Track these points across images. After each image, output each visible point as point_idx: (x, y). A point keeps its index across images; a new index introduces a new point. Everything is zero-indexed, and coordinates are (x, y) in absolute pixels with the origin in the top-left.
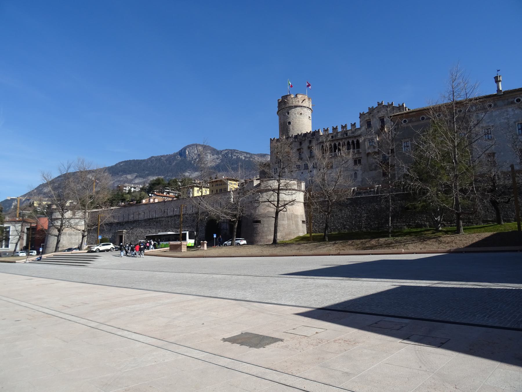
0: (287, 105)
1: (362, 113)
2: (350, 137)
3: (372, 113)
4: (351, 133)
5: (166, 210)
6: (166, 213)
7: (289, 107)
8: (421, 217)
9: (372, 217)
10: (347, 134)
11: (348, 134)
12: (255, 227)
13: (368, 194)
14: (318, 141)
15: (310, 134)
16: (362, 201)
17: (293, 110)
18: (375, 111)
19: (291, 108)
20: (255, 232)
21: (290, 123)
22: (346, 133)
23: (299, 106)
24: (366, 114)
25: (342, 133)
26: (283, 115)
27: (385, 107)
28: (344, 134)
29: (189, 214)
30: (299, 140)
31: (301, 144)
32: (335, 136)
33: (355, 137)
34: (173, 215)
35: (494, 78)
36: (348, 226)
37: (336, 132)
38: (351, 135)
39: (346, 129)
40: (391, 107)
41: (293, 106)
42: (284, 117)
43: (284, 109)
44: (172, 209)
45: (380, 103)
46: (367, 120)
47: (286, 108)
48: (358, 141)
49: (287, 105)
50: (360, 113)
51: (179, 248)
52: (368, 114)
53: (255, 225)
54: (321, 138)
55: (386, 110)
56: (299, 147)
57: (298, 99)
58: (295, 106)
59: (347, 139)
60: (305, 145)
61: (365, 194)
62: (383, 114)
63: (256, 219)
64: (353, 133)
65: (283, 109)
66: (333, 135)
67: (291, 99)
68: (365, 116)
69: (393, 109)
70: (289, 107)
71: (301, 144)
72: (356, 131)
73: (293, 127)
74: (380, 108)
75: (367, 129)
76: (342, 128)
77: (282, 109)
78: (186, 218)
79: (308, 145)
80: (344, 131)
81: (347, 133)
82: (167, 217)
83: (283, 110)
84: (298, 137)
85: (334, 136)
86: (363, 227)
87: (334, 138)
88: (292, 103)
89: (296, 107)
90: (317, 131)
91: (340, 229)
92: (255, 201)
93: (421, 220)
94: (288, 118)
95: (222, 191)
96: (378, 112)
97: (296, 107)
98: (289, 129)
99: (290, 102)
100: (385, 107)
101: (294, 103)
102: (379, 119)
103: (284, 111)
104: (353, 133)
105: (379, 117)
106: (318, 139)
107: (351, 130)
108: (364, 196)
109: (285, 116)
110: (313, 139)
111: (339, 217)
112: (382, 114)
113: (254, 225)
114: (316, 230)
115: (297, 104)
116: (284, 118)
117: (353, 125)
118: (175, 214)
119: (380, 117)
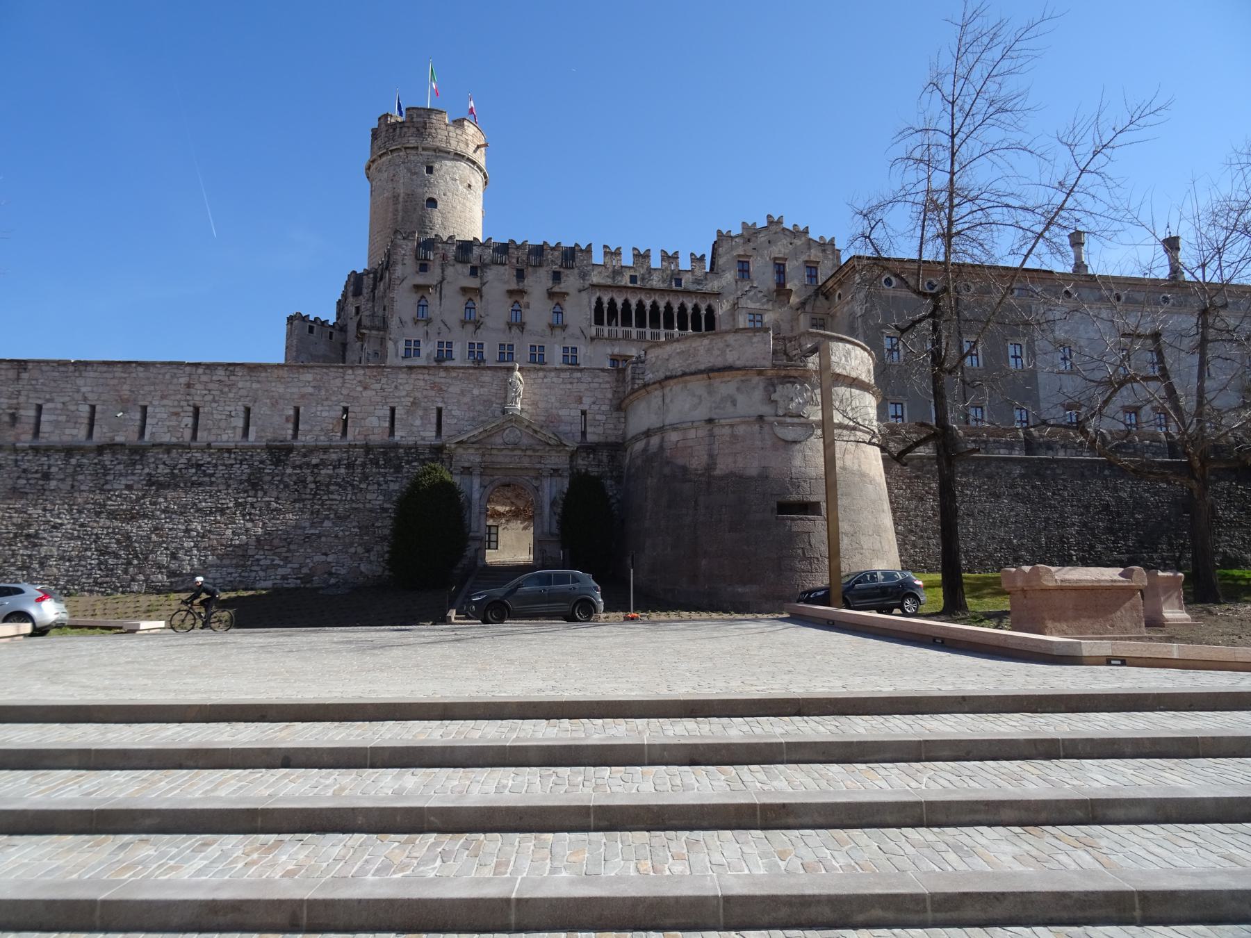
0: (429, 142)
1: (724, 233)
2: (688, 293)
3: (753, 239)
4: (693, 283)
5: (32, 413)
6: (26, 428)
7: (435, 150)
8: (1229, 536)
9: (1098, 527)
10: (679, 282)
11: (683, 282)
12: (795, 529)
13: (1074, 451)
14: (584, 280)
15: (556, 253)
16: (1058, 471)
17: (449, 163)
18: (762, 238)
19: (442, 154)
20: (800, 551)
21: (432, 203)
22: (677, 277)
23: (468, 159)
24: (737, 240)
25: (665, 276)
26: (409, 170)
27: (787, 232)
28: (671, 278)
29: (220, 450)
30: (514, 261)
31: (520, 275)
32: (643, 279)
33: (705, 295)
34: (88, 444)
35: (291, 319)
36: (1026, 550)
37: (645, 267)
38: (693, 287)
39: (677, 265)
40: (803, 239)
41: (449, 153)
42: (415, 177)
43: (414, 152)
44: (85, 409)
45: (776, 219)
46: (739, 256)
47: (424, 149)
48: (710, 310)
49: (429, 142)
50: (719, 232)
51: (1118, 607)
52: (742, 241)
53: (793, 520)
54: (595, 273)
55: (791, 244)
56: (514, 286)
57: (467, 134)
58: (456, 154)
59: (666, 294)
60: (538, 283)
61: (1065, 452)
62: (783, 250)
63: (794, 497)
64: (697, 282)
65: (408, 148)
66: (637, 274)
67: (444, 127)
68: (734, 243)
69: (809, 244)
70: (435, 150)
71: (520, 275)
72: (706, 279)
73: (444, 218)
74: (776, 233)
75: (739, 283)
76: (663, 260)
77: (406, 148)
78: (198, 466)
79: (550, 284)
80: (673, 271)
81: (681, 280)
82: (32, 448)
83: (408, 151)
84: (511, 251)
85: (638, 279)
86: (1074, 557)
87: (639, 283)
88: (448, 142)
89: (459, 156)
90: (584, 248)
91: (1000, 559)
92: (784, 415)
93: (1230, 546)
94: (426, 184)
95: (360, 363)
96: (769, 242)
97: (459, 156)
98: (431, 222)
99: (442, 134)
100: (787, 232)
101: (453, 142)
102: (771, 263)
103: (412, 158)
104: (699, 284)
105: (772, 257)
106: (584, 276)
107: (692, 271)
108: (1061, 455)
109: (415, 173)
110: (568, 272)
111: (994, 518)
112: (780, 250)
113: (789, 522)
114: (914, 561)
115: (461, 148)
116: (412, 180)
117: (697, 260)
118: (105, 440)
119: (775, 259)
